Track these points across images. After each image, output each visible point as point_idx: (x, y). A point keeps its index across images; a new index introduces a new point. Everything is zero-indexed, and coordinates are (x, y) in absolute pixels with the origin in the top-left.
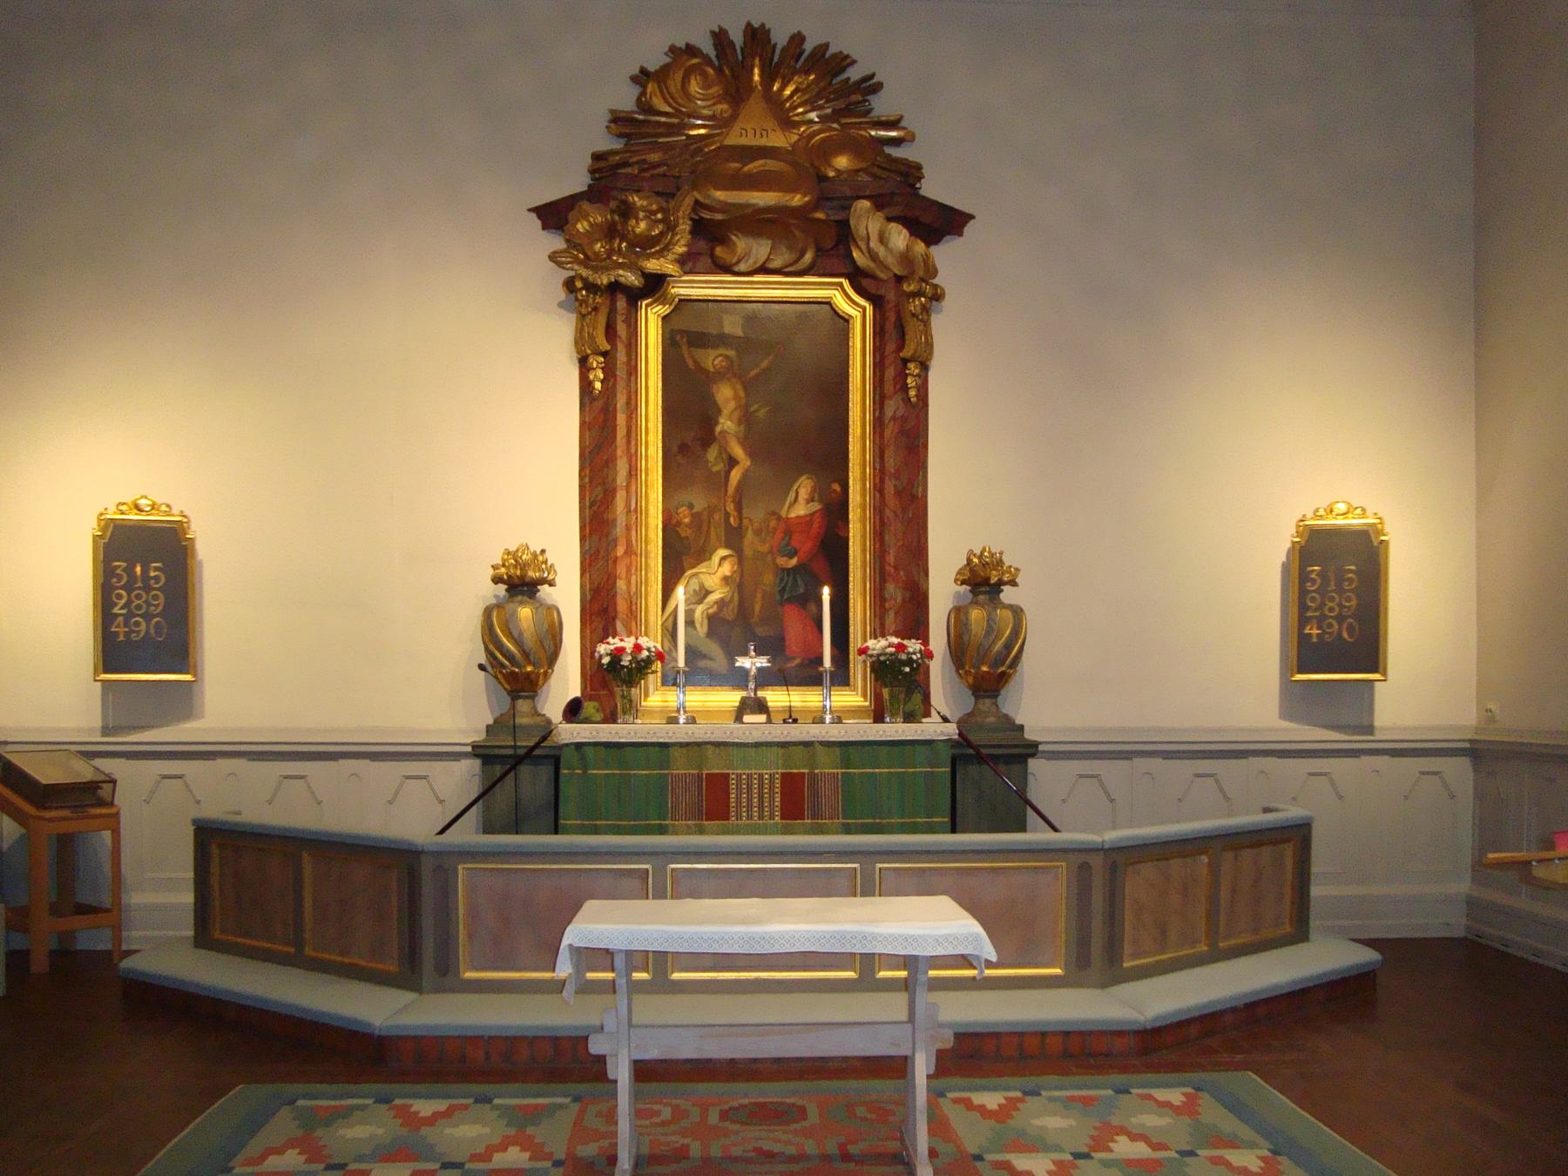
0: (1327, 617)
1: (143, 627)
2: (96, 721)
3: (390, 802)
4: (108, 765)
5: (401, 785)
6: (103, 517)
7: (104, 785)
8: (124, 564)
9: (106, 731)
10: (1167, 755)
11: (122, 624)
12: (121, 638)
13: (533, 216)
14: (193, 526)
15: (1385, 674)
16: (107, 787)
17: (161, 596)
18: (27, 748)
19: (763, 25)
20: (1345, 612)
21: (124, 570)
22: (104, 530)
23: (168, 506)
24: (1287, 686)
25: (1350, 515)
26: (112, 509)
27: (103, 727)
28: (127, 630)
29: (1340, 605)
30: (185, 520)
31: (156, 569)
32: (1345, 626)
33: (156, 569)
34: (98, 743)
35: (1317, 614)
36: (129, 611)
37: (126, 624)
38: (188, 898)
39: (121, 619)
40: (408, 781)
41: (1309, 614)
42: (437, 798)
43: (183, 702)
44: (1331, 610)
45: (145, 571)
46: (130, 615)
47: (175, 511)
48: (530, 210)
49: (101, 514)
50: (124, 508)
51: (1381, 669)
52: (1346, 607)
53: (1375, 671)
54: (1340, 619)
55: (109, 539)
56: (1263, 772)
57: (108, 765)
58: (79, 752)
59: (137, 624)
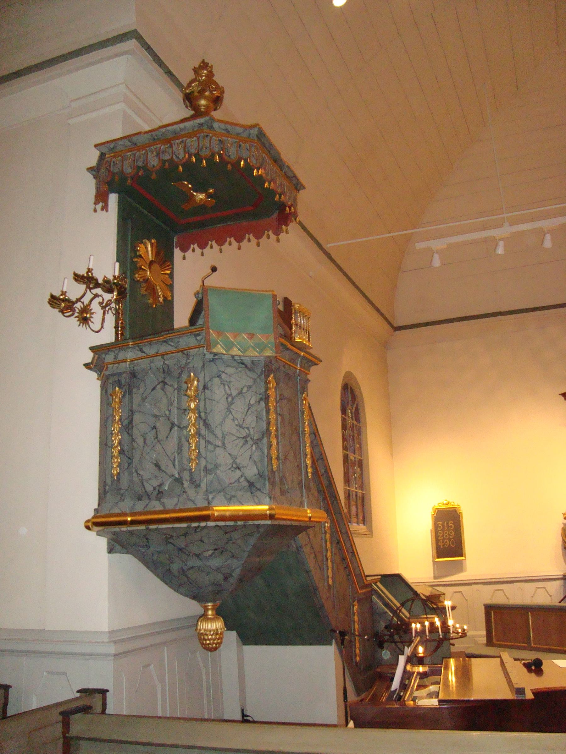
0: (445, 539)
1: (448, 543)
2: (432, 575)
3: (532, 597)
4: (441, 589)
5: (536, 590)
6: (434, 508)
7: (442, 595)
8: (441, 523)
9: (435, 578)
10: (526, 581)
11: (442, 542)
12: (442, 547)
13: (561, 396)
14: (462, 508)
15: (465, 557)
16: (443, 596)
17: (453, 533)
18: (419, 584)
19: (98, 379)
20: (451, 537)
21: (441, 525)
22: (435, 512)
23: (453, 503)
24: (434, 563)
25: (449, 505)
26: (437, 505)
27: (434, 577)
28: (443, 544)
29: (449, 534)
30: (459, 507)
31: (451, 523)
32: (451, 542)
33: (451, 523)
34: (433, 582)
35: (442, 538)
36: (443, 538)
37: (443, 542)
38: (484, 633)
39: (441, 541)
40: (496, 591)
41: (440, 538)
42: (549, 594)
43: (459, 567)
44: (446, 536)
45: (447, 524)
46: (444, 539)
47: (456, 504)
48: (560, 394)
49: (434, 507)
50: (440, 504)
51: (463, 555)
52: (451, 535)
53: (462, 556)
54: (449, 539)
55: (437, 515)
56: (478, 590)
57: (441, 589)
58: (428, 585)
59: (446, 542)
